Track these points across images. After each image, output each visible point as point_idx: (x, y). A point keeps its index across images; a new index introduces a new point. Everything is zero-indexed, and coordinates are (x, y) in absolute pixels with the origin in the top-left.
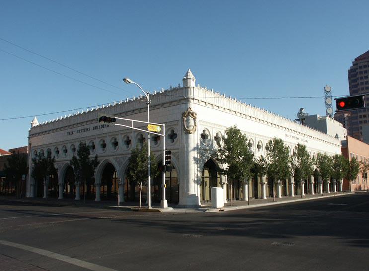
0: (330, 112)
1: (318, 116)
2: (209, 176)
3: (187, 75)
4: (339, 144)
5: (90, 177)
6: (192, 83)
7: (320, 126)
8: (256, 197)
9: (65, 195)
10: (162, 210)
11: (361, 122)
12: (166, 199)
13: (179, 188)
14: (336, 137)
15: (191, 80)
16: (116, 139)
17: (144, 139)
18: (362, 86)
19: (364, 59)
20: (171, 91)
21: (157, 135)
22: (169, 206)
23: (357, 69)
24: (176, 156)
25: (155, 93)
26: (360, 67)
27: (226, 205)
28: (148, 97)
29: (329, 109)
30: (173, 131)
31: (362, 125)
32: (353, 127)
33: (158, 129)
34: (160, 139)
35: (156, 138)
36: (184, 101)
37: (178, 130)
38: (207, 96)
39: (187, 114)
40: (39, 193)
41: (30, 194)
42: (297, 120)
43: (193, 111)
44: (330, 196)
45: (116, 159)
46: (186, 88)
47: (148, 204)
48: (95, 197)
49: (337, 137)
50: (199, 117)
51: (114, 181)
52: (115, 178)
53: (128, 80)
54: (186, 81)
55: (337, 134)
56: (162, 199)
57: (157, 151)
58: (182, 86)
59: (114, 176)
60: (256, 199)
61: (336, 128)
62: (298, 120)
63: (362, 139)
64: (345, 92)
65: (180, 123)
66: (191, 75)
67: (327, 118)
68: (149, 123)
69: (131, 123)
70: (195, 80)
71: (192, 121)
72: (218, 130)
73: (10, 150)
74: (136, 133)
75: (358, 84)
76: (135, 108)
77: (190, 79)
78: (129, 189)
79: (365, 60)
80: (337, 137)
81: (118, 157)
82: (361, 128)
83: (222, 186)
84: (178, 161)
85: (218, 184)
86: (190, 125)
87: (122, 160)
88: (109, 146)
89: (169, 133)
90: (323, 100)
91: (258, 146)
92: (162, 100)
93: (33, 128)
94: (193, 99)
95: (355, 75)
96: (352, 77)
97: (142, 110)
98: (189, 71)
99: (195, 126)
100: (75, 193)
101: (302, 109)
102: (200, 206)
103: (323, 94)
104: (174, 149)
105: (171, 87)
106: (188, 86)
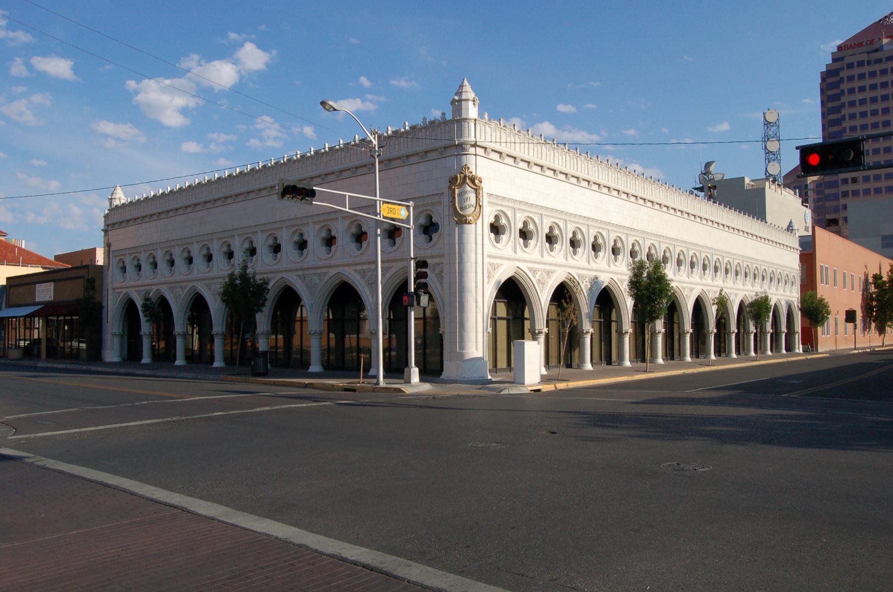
0: (774, 169)
1: (747, 180)
2: (508, 314)
3: (459, 93)
4: (796, 244)
5: (270, 320)
6: (472, 111)
7: (747, 201)
8: (609, 362)
9: (191, 357)
10: (408, 390)
11: (845, 194)
12: (416, 365)
13: (442, 341)
14: (788, 230)
15: (471, 103)
16: (302, 235)
17: (366, 233)
18: (853, 110)
19: (860, 44)
20: (426, 128)
21: (395, 225)
22: (421, 380)
23: (842, 69)
24: (437, 270)
25: (390, 133)
26: (850, 66)
27: (545, 379)
28: (375, 142)
29: (772, 163)
30: (430, 218)
31: (849, 201)
32: (828, 204)
33: (402, 213)
34: (400, 235)
35: (393, 232)
36: (454, 151)
37: (441, 216)
38: (504, 140)
39: (461, 179)
40: (132, 353)
41: (112, 353)
42: (695, 189)
43: (474, 173)
44: (784, 360)
45: (303, 278)
46: (459, 121)
47: (376, 377)
48: (175, 359)
49: (790, 228)
50: (487, 187)
51: (297, 326)
52: (302, 320)
53: (331, 103)
54: (457, 104)
55: (791, 223)
56: (407, 364)
57: (396, 261)
58: (449, 117)
59: (299, 315)
60: (610, 367)
61: (787, 207)
62: (701, 189)
63: (846, 232)
64: (815, 136)
65: (446, 200)
66: (469, 93)
67: (767, 183)
68: (378, 198)
69: (337, 199)
70: (477, 102)
71: (472, 196)
72: (527, 214)
73: (57, 258)
74: (347, 222)
75: (843, 105)
76: (349, 163)
77: (467, 100)
78: (333, 344)
79: (861, 49)
80: (790, 228)
81: (310, 277)
82: (845, 207)
83: (534, 337)
84: (441, 283)
85: (527, 334)
86: (467, 203)
87: (318, 281)
88: (288, 248)
89: (422, 220)
90: (760, 145)
91: (613, 250)
92: (405, 148)
93: (114, 210)
94: (475, 145)
95: (836, 85)
96: (828, 89)
97: (361, 171)
98: (466, 83)
99: (479, 205)
100: (212, 351)
101: (708, 165)
102: (491, 382)
103: (760, 130)
104: (433, 257)
105: (424, 119)
106: (464, 116)
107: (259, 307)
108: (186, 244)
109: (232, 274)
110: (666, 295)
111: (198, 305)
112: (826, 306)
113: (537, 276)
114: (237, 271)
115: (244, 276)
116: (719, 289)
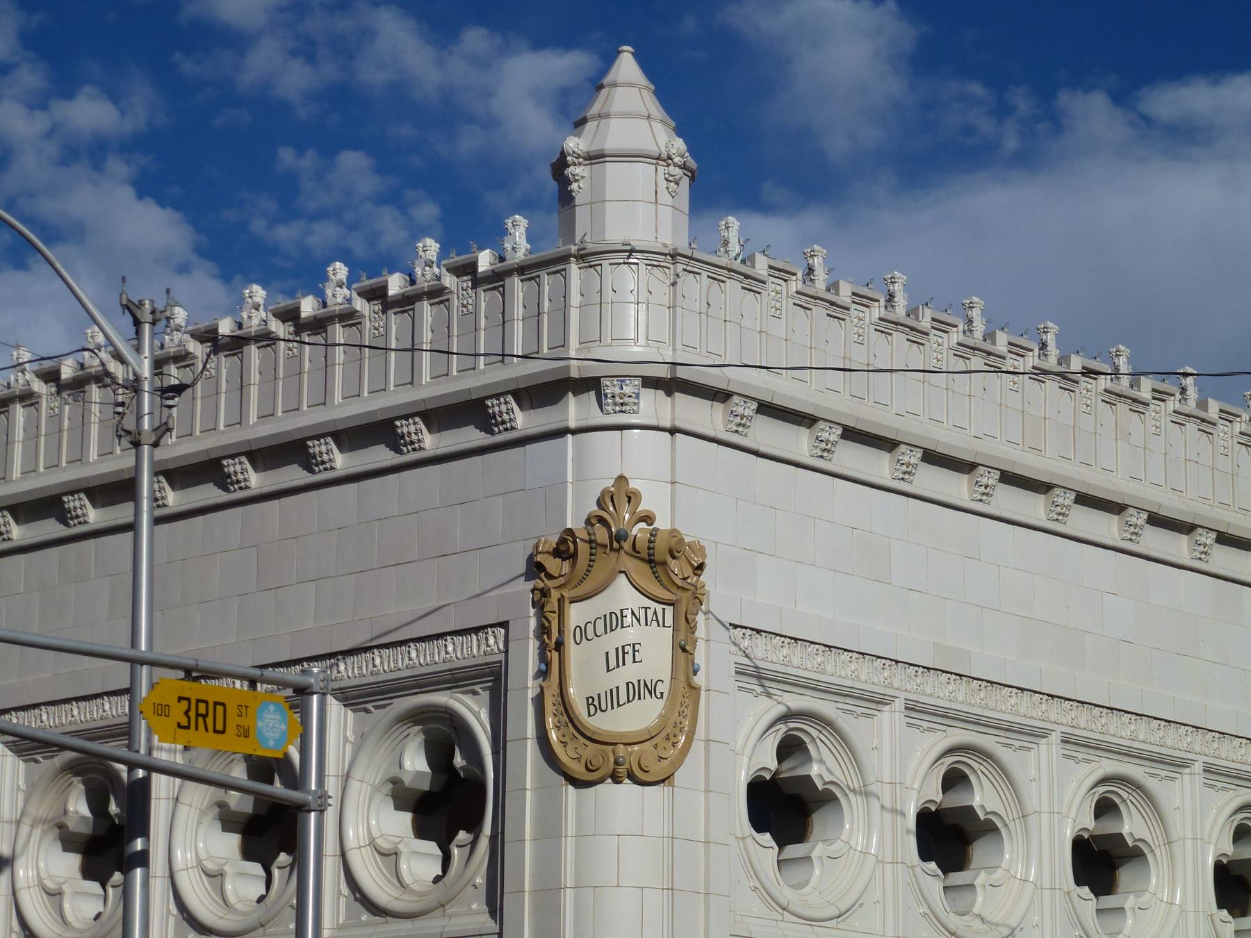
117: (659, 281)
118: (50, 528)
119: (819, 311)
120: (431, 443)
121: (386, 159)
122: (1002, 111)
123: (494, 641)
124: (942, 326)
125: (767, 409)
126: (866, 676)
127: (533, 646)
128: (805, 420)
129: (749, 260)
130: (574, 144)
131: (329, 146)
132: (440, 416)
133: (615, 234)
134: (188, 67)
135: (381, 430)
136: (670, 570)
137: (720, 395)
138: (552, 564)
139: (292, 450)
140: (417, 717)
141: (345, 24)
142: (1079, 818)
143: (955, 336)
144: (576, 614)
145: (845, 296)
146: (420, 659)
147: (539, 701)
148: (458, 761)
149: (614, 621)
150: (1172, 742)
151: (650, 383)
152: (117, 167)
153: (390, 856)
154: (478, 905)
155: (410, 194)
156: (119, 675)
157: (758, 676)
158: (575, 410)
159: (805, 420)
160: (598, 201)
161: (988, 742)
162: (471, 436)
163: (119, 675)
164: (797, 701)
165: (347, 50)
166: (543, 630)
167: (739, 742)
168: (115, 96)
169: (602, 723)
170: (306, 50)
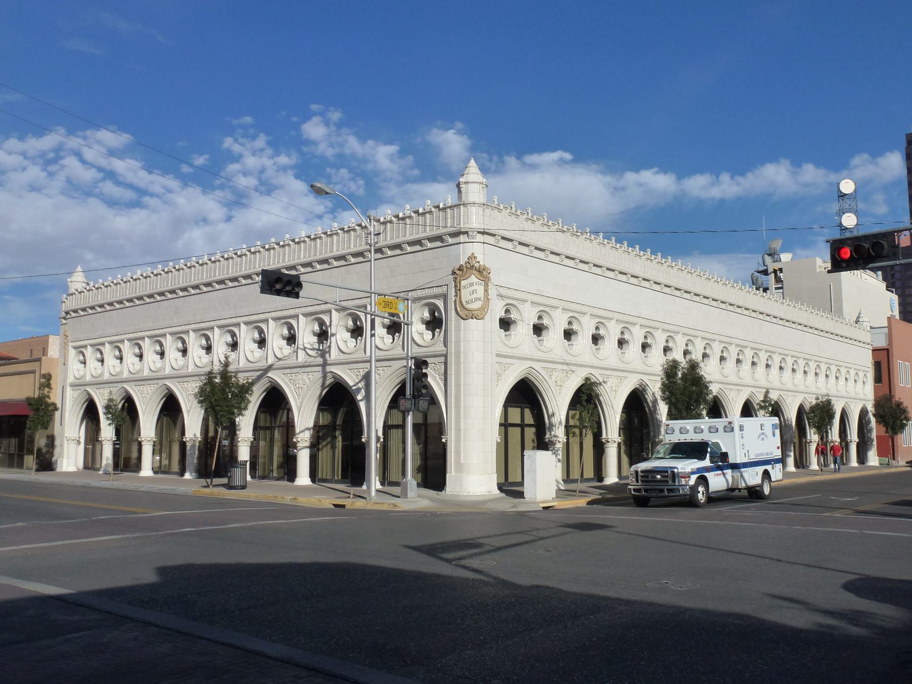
107: (241, 409)
108: (627, 323)
109: (210, 373)
110: (705, 401)
111: (586, 398)
112: (904, 411)
113: (553, 378)
114: (217, 368)
115: (225, 375)
116: (764, 390)
117: (480, 210)
118: (343, 263)
119: (513, 216)
120: (429, 245)
121: (351, 170)
122: (491, 160)
123: (445, 288)
124: (538, 219)
125: (503, 238)
126: (523, 296)
127: (453, 290)
128: (511, 240)
129: (499, 205)
130: (461, 180)
131: (338, 168)
132: (432, 239)
133: (471, 200)
134: (305, 149)
135: (418, 242)
136: (482, 273)
137: (494, 235)
138: (458, 272)
139: (398, 246)
140: (427, 305)
141: (340, 139)
142: (565, 326)
143: (541, 222)
144: (463, 283)
145: (519, 213)
146: (428, 292)
147: (455, 302)
148: (436, 314)
149: (471, 285)
150: (584, 309)
151: (479, 232)
152: (290, 172)
153: (421, 334)
154: (442, 345)
155: (357, 178)
156: (369, 295)
157: (501, 296)
158: (462, 238)
159: (511, 240)
160: (467, 192)
161: (627, 326)
162: (439, 244)
163: (369, 295)
164: (509, 301)
165: (341, 145)
166: (456, 286)
167: (497, 311)
168: (288, 156)
169: (468, 306)
170: (332, 145)
